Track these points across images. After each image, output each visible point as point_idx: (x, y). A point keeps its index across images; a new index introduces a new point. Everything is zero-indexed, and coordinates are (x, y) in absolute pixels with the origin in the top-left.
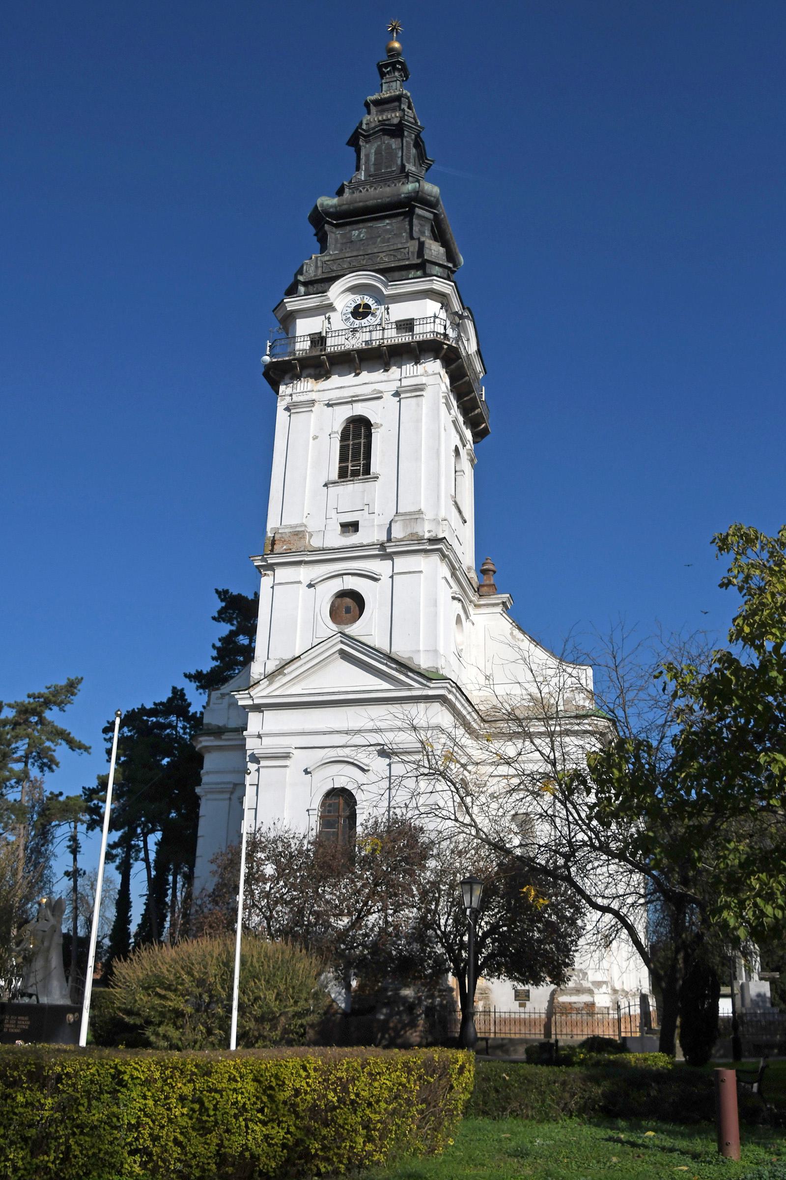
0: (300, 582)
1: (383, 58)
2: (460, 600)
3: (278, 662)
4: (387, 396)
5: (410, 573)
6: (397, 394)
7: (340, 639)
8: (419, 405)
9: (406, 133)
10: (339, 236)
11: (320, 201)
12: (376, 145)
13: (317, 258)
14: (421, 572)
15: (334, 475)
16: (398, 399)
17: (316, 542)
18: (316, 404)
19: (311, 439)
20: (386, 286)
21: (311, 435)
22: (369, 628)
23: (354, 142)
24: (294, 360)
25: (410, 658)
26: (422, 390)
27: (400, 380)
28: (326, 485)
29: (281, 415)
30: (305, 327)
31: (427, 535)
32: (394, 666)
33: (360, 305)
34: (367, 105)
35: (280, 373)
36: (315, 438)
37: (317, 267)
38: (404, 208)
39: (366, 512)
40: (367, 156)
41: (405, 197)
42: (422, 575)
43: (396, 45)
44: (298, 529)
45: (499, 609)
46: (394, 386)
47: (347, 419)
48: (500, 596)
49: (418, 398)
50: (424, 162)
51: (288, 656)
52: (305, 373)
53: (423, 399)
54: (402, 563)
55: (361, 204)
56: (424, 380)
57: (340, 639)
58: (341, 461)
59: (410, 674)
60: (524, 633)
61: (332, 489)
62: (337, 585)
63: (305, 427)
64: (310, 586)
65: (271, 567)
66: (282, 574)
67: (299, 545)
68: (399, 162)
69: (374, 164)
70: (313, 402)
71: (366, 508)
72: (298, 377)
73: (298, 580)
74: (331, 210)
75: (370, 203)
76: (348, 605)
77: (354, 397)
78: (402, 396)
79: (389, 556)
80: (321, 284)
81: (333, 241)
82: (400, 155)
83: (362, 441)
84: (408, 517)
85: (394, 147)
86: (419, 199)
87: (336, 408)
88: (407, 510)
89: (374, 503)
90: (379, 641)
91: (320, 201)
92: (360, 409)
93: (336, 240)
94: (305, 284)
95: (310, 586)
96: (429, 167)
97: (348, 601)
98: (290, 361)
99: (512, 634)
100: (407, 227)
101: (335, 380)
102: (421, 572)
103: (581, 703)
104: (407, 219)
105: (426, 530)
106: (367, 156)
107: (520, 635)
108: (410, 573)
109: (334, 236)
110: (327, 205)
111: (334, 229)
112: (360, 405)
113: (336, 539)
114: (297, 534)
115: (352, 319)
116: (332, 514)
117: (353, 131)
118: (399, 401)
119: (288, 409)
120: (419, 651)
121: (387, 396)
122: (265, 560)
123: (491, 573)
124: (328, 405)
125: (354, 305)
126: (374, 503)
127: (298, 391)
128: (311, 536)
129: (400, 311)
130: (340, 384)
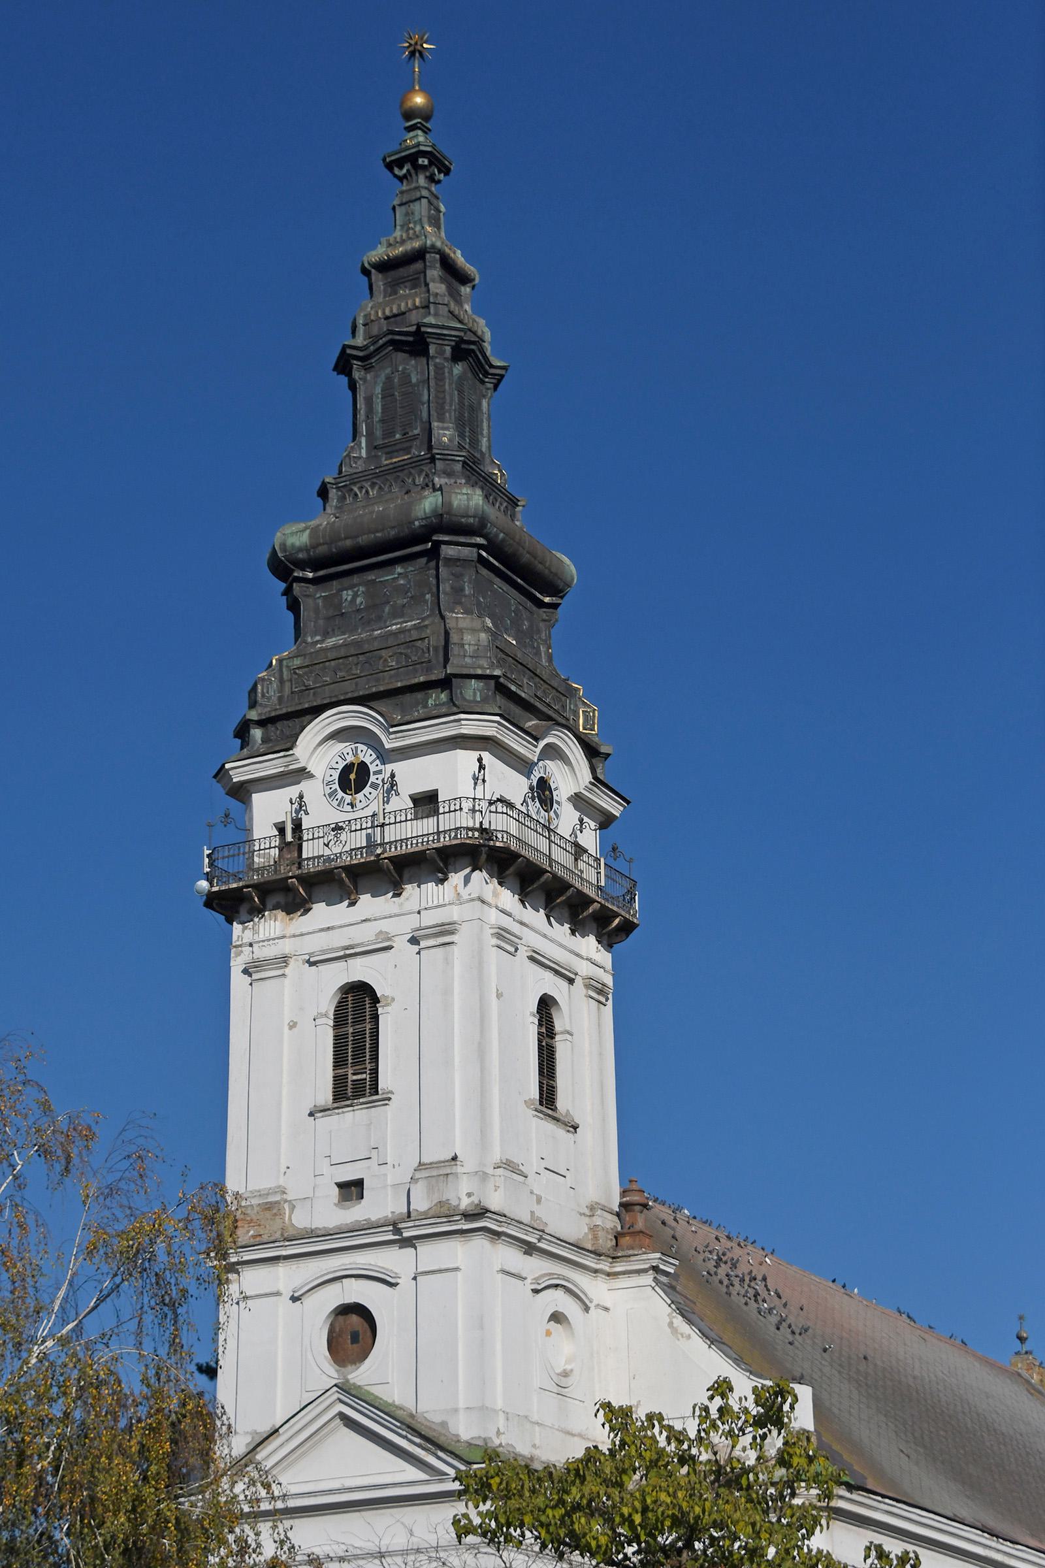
0: (278, 1294)
2: (557, 1286)
3: (248, 1439)
4: (401, 944)
5: (440, 1271)
6: (414, 941)
7: (337, 1396)
8: (448, 961)
9: (432, 350)
10: (320, 602)
11: (278, 538)
12: (383, 377)
13: (280, 661)
14: (457, 1269)
15: (325, 1093)
16: (416, 948)
17: (300, 1220)
18: (292, 962)
19: (286, 1028)
20: (386, 730)
21: (287, 1022)
22: (383, 1372)
23: (343, 365)
24: (247, 887)
25: (444, 1424)
26: (452, 933)
27: (419, 912)
28: (311, 1114)
29: (238, 981)
30: (268, 811)
31: (465, 1203)
32: (417, 1440)
33: (352, 764)
34: (366, 272)
35: (232, 905)
36: (293, 1025)
37: (282, 681)
38: (419, 543)
39: (373, 1163)
40: (369, 401)
41: (421, 526)
42: (459, 1274)
43: (419, 100)
44: (271, 1199)
45: (648, 1279)
46: (408, 925)
47: (341, 988)
48: (645, 1257)
49: (448, 948)
50: (486, 374)
51: (265, 1428)
52: (271, 901)
54: (432, 1254)
55: (348, 543)
56: (454, 913)
57: (337, 1396)
58: (339, 1061)
59: (440, 1454)
60: (690, 1322)
61: (323, 1122)
62: (336, 1296)
63: (276, 997)
64: (294, 1299)
65: (233, 1268)
67: (272, 1229)
68: (425, 415)
69: (382, 421)
70: (284, 960)
71: (374, 1154)
72: (258, 911)
73: (274, 1290)
74: (300, 556)
75: (363, 540)
76: (353, 1332)
77: (347, 948)
78: (423, 944)
80: (283, 726)
81: (312, 614)
82: (425, 398)
83: (368, 1026)
84: (435, 1173)
85: (414, 380)
86: (446, 525)
88: (435, 1159)
89: (388, 1142)
90: (397, 1393)
91: (278, 538)
93: (317, 610)
94: (261, 723)
96: (499, 381)
97: (354, 1319)
98: (240, 889)
99: (671, 1324)
100: (433, 581)
102: (457, 1269)
104: (433, 564)
105: (462, 1195)
106: (369, 401)
108: (440, 1271)
109: (314, 599)
110: (293, 545)
112: (358, 961)
113: (328, 1213)
114: (268, 1207)
115: (340, 794)
116: (324, 1167)
117: (337, 354)
118: (419, 953)
119: (246, 972)
120: (456, 1410)
121: (401, 944)
123: (638, 1208)
125: (336, 775)
126: (388, 1142)
127: (262, 937)
128: (293, 1208)
129: (415, 775)
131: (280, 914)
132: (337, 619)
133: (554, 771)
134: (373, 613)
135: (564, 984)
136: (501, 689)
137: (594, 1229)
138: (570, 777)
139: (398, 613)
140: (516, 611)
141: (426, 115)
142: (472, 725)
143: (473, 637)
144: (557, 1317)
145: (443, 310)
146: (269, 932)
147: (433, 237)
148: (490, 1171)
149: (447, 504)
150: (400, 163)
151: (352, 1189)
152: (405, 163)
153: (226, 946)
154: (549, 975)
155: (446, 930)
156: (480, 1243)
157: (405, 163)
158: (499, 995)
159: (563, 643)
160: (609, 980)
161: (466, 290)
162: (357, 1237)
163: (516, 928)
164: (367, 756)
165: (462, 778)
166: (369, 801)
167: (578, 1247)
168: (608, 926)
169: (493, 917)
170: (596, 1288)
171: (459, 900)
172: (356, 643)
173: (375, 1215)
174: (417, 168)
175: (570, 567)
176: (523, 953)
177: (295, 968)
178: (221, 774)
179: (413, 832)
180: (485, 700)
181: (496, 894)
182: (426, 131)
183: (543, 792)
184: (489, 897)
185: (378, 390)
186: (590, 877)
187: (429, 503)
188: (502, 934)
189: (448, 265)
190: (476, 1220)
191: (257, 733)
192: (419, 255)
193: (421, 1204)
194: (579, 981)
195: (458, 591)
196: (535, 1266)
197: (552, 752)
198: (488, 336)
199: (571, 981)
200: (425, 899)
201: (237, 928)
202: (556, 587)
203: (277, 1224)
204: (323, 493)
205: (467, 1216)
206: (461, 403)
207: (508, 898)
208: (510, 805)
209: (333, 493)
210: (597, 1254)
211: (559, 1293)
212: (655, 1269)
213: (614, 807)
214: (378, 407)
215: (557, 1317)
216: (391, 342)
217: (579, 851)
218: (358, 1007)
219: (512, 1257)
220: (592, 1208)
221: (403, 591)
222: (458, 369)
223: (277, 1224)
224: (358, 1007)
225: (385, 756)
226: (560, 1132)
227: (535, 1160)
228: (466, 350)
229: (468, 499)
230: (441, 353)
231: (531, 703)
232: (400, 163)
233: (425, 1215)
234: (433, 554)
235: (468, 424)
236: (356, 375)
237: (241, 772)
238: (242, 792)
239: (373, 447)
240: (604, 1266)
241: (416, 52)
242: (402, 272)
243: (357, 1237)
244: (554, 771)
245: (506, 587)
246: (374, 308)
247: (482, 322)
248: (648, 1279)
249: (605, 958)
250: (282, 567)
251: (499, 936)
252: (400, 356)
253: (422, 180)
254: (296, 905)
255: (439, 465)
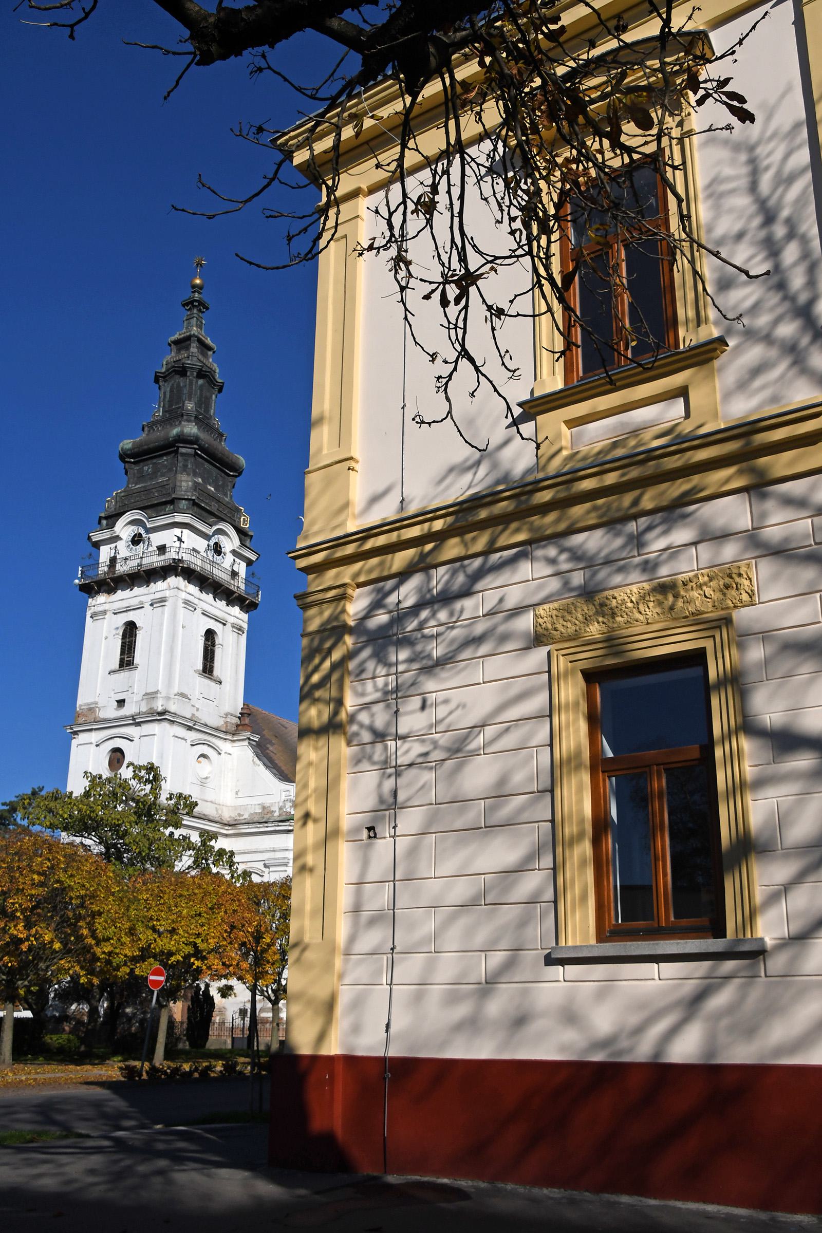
1: (187, 295)
4: (147, 606)
6: (152, 605)
8: (163, 613)
9: (188, 374)
15: (116, 665)
17: (102, 715)
29: (88, 620)
30: (105, 553)
31: (160, 709)
34: (170, 345)
35: (91, 589)
37: (116, 502)
38: (170, 447)
43: (198, 281)
45: (246, 743)
53: (166, 608)
54: (146, 729)
55: (146, 447)
56: (167, 594)
58: (122, 653)
60: (260, 760)
64: (97, 746)
65: (76, 733)
66: (82, 738)
70: (105, 612)
75: (151, 446)
79: (138, 724)
80: (112, 519)
87: (119, 615)
92: (131, 616)
95: (97, 746)
97: (119, 754)
101: (120, 594)
103: (288, 810)
106: (165, 393)
107: (258, 762)
111: (133, 466)
112: (132, 612)
113: (109, 711)
114: (90, 709)
116: (112, 694)
121: (147, 606)
122: (71, 729)
124: (115, 614)
126: (135, 684)
129: (157, 539)
130: (123, 597)
131: (106, 595)
132: (141, 477)
133: (222, 540)
134: (154, 475)
135: (221, 625)
136: (195, 503)
137: (226, 723)
138: (231, 542)
139: (163, 475)
140: (216, 477)
141: (200, 287)
142: (179, 518)
143: (185, 483)
144: (203, 756)
145: (195, 359)
146: (101, 601)
147: (195, 330)
148: (172, 696)
149: (182, 431)
150: (187, 304)
151: (121, 703)
152: (189, 304)
153: (85, 606)
154: (213, 621)
155: (163, 600)
156: (165, 725)
157: (189, 304)
158: (183, 627)
159: (237, 493)
160: (245, 626)
161: (210, 353)
162: (118, 723)
163: (196, 601)
164: (142, 531)
165: (183, 541)
166: (140, 547)
167: (217, 729)
168: (248, 606)
169: (183, 595)
170: (225, 746)
171: (170, 588)
172: (145, 487)
173: (128, 714)
174: (194, 306)
175: (242, 461)
176: (199, 611)
177: (109, 615)
178: (89, 538)
179: (156, 561)
180: (188, 508)
181: (186, 587)
182: (200, 293)
183: (217, 549)
184: (182, 587)
185: (168, 389)
186: (239, 585)
187: (175, 431)
188: (187, 602)
189: (201, 342)
190: (162, 716)
191: (104, 522)
192: (188, 338)
193: (144, 709)
194: (229, 625)
195: (185, 466)
196: (192, 736)
197: (220, 532)
198: (217, 371)
199: (224, 624)
200: (159, 587)
201: (90, 600)
202: (239, 471)
203: (93, 716)
204: (143, 429)
205: (160, 714)
206: (201, 394)
207: (193, 589)
208: (198, 552)
209: (146, 429)
210: (226, 732)
211: (206, 746)
212: (249, 739)
213: (253, 557)
214: (168, 396)
215: (203, 756)
216: (174, 371)
217: (234, 574)
218: (130, 629)
219: (181, 732)
220: (226, 715)
221: (166, 466)
222: (201, 382)
223: (93, 716)
224: (130, 629)
225: (149, 531)
226: (212, 684)
227: (197, 693)
228: (204, 374)
229: (191, 429)
230: (192, 374)
231: (208, 511)
232: (187, 304)
233: (145, 713)
234: (176, 452)
235: (204, 403)
236: (161, 384)
237: (96, 537)
238: (97, 545)
239: (164, 411)
240: (229, 737)
241: (199, 264)
242: (183, 345)
243: (118, 723)
244: (222, 540)
245: (211, 467)
246: (171, 356)
247: (215, 365)
248: (246, 743)
249: (245, 617)
250: (123, 457)
251: (185, 603)
252: (177, 376)
253: (195, 311)
254: (111, 591)
255: (185, 417)
